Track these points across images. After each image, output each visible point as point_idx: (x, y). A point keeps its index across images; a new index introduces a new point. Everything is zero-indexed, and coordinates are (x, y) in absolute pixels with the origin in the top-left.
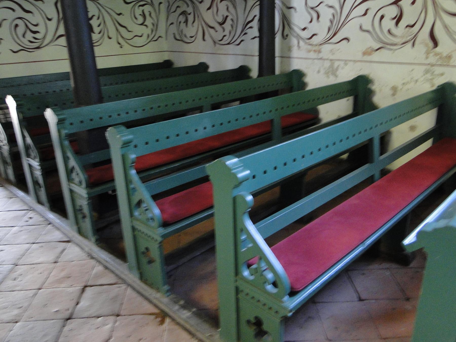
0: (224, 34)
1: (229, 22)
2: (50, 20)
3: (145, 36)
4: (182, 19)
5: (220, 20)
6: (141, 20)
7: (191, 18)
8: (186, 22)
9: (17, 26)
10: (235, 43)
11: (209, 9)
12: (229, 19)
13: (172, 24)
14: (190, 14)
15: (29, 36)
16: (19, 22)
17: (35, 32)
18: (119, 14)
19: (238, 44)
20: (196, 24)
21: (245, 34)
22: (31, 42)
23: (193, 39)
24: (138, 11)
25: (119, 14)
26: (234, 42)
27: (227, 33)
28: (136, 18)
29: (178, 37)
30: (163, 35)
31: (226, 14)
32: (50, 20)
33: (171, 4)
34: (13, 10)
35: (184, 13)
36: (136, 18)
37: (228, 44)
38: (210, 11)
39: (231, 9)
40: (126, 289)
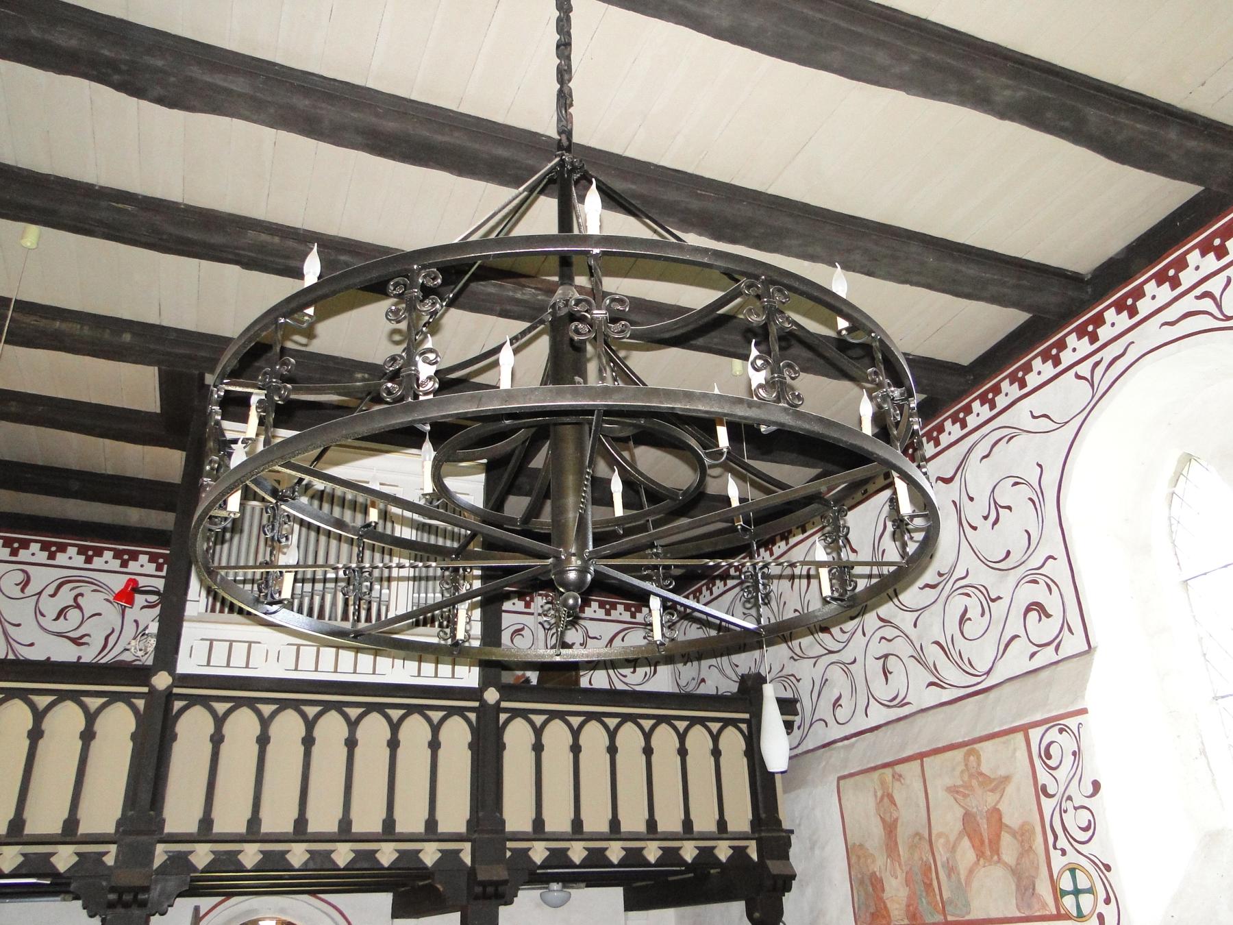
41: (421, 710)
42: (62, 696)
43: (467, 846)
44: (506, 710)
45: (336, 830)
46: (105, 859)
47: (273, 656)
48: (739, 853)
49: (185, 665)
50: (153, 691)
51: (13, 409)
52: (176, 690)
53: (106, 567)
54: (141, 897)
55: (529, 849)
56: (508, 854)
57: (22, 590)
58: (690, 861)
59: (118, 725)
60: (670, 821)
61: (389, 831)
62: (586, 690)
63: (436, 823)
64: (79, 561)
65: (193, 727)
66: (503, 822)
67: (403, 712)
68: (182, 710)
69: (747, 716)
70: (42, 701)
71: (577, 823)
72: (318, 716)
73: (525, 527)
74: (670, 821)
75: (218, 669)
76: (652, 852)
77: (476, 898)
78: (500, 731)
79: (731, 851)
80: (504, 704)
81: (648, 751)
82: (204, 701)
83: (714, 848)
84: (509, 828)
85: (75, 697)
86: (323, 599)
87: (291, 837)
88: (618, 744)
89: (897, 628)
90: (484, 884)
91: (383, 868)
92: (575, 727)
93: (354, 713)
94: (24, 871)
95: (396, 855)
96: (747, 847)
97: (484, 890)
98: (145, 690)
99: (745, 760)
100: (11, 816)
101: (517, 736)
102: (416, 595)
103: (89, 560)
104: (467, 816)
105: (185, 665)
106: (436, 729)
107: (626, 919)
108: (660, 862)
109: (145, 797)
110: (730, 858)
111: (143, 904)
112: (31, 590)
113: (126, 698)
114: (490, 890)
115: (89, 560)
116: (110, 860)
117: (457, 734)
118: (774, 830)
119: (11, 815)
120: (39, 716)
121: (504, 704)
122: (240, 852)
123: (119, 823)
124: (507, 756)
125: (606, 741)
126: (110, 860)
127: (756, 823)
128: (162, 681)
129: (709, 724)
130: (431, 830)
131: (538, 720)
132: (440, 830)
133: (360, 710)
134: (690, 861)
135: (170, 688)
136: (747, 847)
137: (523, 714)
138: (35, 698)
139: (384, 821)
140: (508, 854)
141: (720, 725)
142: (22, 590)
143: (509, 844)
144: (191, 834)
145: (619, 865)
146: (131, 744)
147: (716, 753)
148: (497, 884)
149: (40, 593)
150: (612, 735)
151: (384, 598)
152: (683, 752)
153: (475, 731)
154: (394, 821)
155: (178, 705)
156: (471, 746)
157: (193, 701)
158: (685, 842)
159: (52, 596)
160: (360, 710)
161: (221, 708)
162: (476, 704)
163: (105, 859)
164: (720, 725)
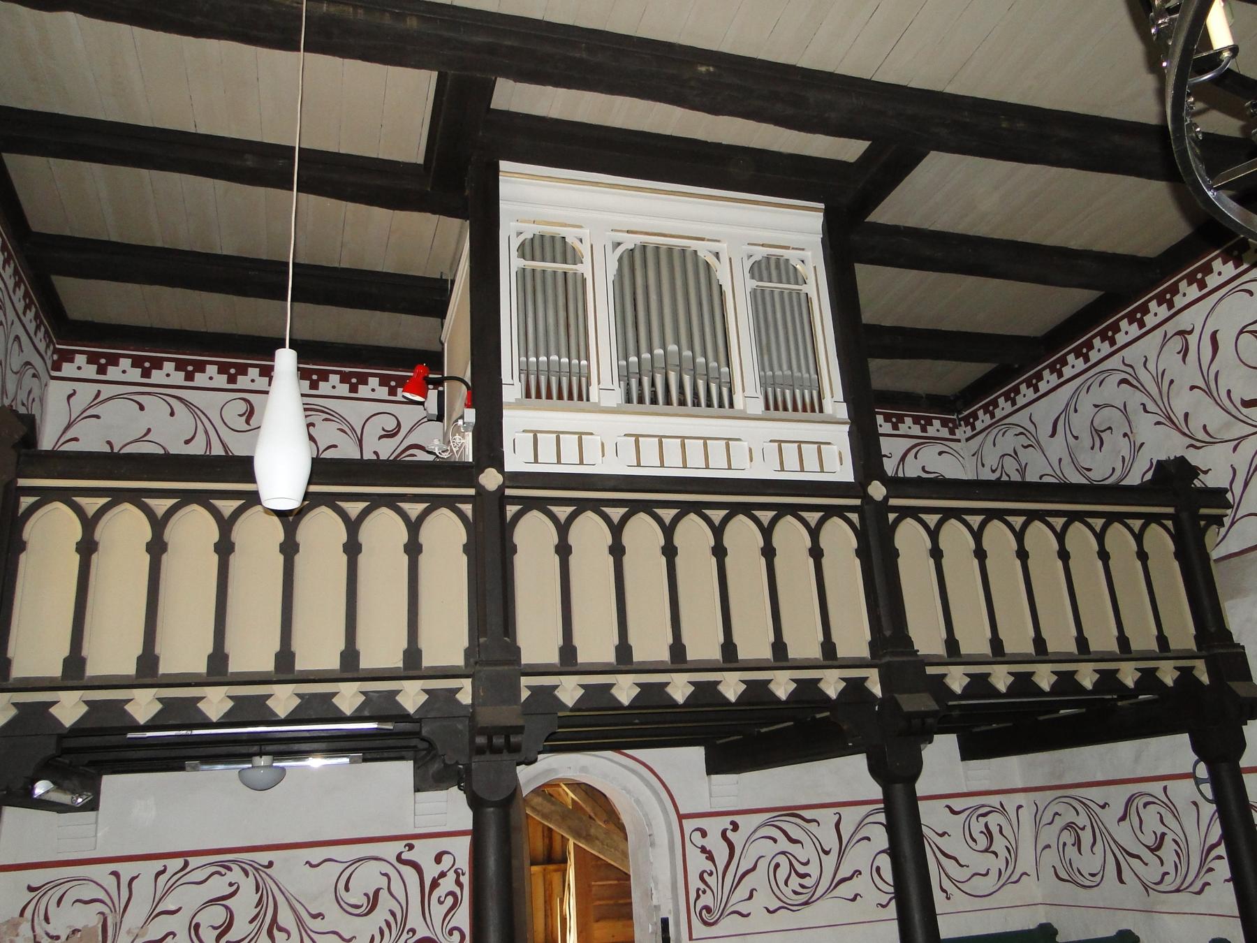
0: (1165, 869)
1: (1169, 845)
2: (827, 853)
3: (994, 874)
4: (1068, 837)
5: (1150, 841)
6: (983, 842)
7: (1086, 837)
8: (1078, 843)
9: (777, 866)
10: (1193, 889)
11: (1122, 819)
12: (1168, 839)
13: (1048, 846)
14: (1083, 829)
15: (795, 882)
16: (782, 860)
17: (803, 876)
18: (942, 835)
19: (1199, 893)
20: (1099, 848)
21: (1211, 870)
22: (795, 892)
23: (1098, 878)
24: (978, 827)
25: (942, 835)
26: (1191, 884)
27: (1169, 867)
28: (974, 840)
29: (1063, 875)
30: (1031, 870)
31: (1160, 829)
32: (827, 853)
33: (1041, 809)
34: (775, 841)
35: (1070, 826)
36: (974, 840)
37: (1178, 891)
38: (1126, 823)
39: (1169, 819)
40: (1022, 471)
41: (697, 508)
42: (118, 497)
43: (467, 684)
44: (515, 500)
45: (401, 665)
46: (458, 696)
47: (610, 450)
48: (1186, 675)
49: (516, 461)
50: (481, 490)
51: (249, 163)
52: (508, 492)
54: (513, 739)
55: (945, 675)
56: (525, 694)
57: (248, 422)
58: (733, 699)
59: (446, 534)
60: (1018, 640)
61: (624, 659)
62: (53, 455)
63: (292, 656)
65: (533, 536)
66: (7, 663)
67: (676, 511)
68: (518, 516)
69: (1171, 510)
70: (161, 506)
71: (729, 648)
72: (572, 518)
74: (1018, 640)
75: (650, 469)
77: (480, 751)
78: (505, 530)
79: (1055, 678)
80: (893, 502)
81: (719, 551)
82: (541, 504)
83: (611, 686)
84: (527, 658)
85: (135, 497)
86: (640, 383)
87: (670, 666)
88: (775, 544)
90: (489, 732)
91: (621, 707)
92: (766, 524)
93: (717, 515)
94: (366, 713)
95: (230, 704)
96: (1193, 668)
97: (490, 739)
98: (472, 492)
99: (858, 561)
100: (210, 650)
102: (523, 359)
104: (465, 643)
105: (516, 461)
106: (669, 531)
107: (710, 781)
109: (495, 620)
110: (842, 694)
111: (515, 749)
113: (450, 503)
116: (465, 698)
117: (840, 538)
118: (903, 654)
119: (139, 651)
120: (158, 524)
121: (893, 502)
122: (335, 694)
123: (468, 653)
124: (521, 563)
125: (404, 536)
126: (465, 698)
127: (1202, 636)
128: (490, 479)
129: (1129, 521)
130: (412, 665)
131: (91, 505)
132: (635, 659)
133: (170, 502)
134: (733, 699)
135: (501, 488)
136: (1193, 668)
137: (913, 513)
138: (151, 502)
139: (617, 648)
140: (525, 694)
141: (938, 517)
143: (525, 681)
144: (52, 679)
146: (465, 558)
147: (936, 553)
148: (508, 731)
150: (767, 532)
151: (584, 371)
152: (816, 553)
153: (860, 534)
154: (293, 655)
155: (26, 501)
156: (467, 549)
157: (529, 504)
158: (619, 677)
160: (170, 502)
161: (354, 508)
162: (858, 502)
163: (458, 696)
164: (938, 517)
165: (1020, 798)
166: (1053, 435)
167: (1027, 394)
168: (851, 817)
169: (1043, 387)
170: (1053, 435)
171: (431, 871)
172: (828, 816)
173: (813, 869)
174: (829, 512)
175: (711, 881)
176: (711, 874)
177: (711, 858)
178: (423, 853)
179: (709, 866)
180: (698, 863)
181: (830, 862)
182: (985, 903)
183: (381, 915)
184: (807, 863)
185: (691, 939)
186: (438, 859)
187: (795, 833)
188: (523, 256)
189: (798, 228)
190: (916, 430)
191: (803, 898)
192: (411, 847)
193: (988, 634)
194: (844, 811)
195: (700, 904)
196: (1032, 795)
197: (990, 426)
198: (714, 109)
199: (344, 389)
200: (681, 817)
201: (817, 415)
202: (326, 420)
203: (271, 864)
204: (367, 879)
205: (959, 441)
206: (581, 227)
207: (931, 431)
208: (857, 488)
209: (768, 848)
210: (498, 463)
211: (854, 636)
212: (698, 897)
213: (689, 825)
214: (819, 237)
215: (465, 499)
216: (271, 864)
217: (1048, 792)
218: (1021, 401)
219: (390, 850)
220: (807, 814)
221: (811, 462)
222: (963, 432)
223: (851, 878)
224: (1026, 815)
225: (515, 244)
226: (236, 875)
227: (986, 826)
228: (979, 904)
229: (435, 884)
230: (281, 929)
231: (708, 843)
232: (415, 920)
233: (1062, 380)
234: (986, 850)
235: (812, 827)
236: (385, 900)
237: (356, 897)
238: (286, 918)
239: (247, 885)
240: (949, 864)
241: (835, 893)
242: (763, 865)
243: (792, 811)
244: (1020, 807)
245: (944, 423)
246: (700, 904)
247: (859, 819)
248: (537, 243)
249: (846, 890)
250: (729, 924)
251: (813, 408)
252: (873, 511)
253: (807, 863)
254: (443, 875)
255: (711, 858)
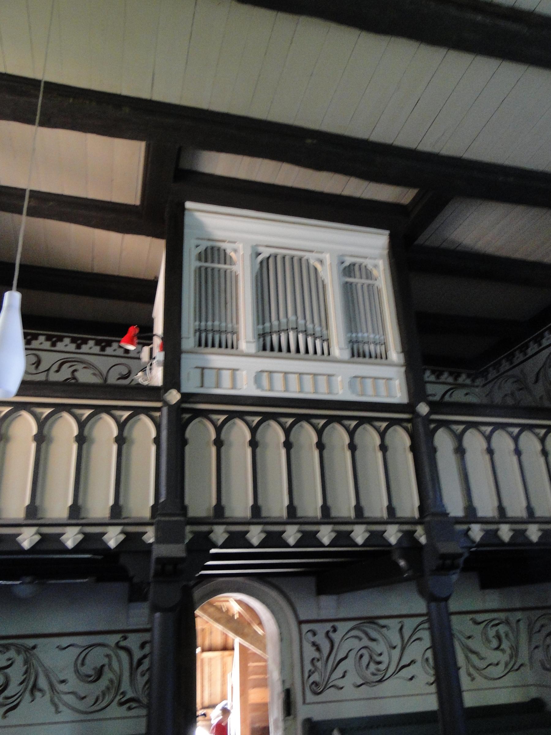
6: (495, 643)
9: (361, 656)
17: (379, 663)
22: (374, 674)
24: (492, 633)
30: (526, 661)
46: (145, 537)
49: (190, 384)
53: (89, 351)
57: (37, 367)
64: (72, 347)
73: (150, 347)
75: (279, 392)
76: (360, 535)
89: (540, 369)
90: (444, 557)
101: (443, 441)
103: (79, 347)
105: (190, 384)
108: (77, 549)
112: (42, 367)
114: (448, 562)
115: (79, 347)
117: (400, 439)
124: (439, 455)
140: (189, 537)
142: (37, 367)
143: (188, 528)
145: (329, 546)
149: (48, 370)
159: (57, 371)
165: (519, 615)
166: (536, 381)
167: (519, 357)
168: (410, 624)
169: (530, 352)
170: (536, 381)
171: (137, 654)
172: (394, 624)
173: (384, 658)
174: (393, 422)
175: (319, 664)
176: (318, 660)
177: (318, 649)
178: (133, 641)
179: (316, 655)
180: (310, 652)
181: (396, 653)
182: (498, 683)
183: (103, 683)
184: (381, 654)
185: (304, 702)
186: (142, 646)
187: (374, 634)
188: (200, 259)
189: (371, 246)
190: (451, 380)
191: (378, 678)
192: (125, 638)
193: (496, 504)
194: (406, 621)
195: (311, 680)
196: (528, 613)
197: (497, 377)
198: (318, 166)
199: (97, 349)
200: (300, 623)
201: (384, 361)
202: (85, 368)
203: (34, 647)
204: (96, 658)
205: (477, 387)
206: (235, 242)
207: (460, 380)
208: (409, 408)
209: (356, 644)
210: (177, 387)
211: (409, 504)
212: (309, 676)
213: (305, 628)
214: (386, 252)
215: (158, 409)
216: (34, 647)
217: (537, 611)
218: (516, 362)
219: (113, 639)
220: (382, 622)
221: (383, 391)
222: (479, 382)
223: (409, 665)
224: (522, 625)
225: (195, 252)
226: (12, 653)
227: (497, 632)
228: (491, 684)
229: (140, 662)
230: (40, 690)
231: (316, 639)
232: (125, 686)
233: (541, 348)
234: (497, 649)
235: (384, 630)
236: (108, 675)
237: (88, 670)
238: (42, 683)
239: (19, 660)
240: (473, 657)
241: (397, 676)
242: (352, 655)
243: (372, 620)
244: (519, 621)
245: (469, 376)
246: (311, 680)
247: (415, 626)
248: (209, 251)
249: (406, 673)
250: (330, 694)
251: (381, 357)
252: (418, 423)
253: (381, 654)
254: (145, 657)
255: (318, 649)
